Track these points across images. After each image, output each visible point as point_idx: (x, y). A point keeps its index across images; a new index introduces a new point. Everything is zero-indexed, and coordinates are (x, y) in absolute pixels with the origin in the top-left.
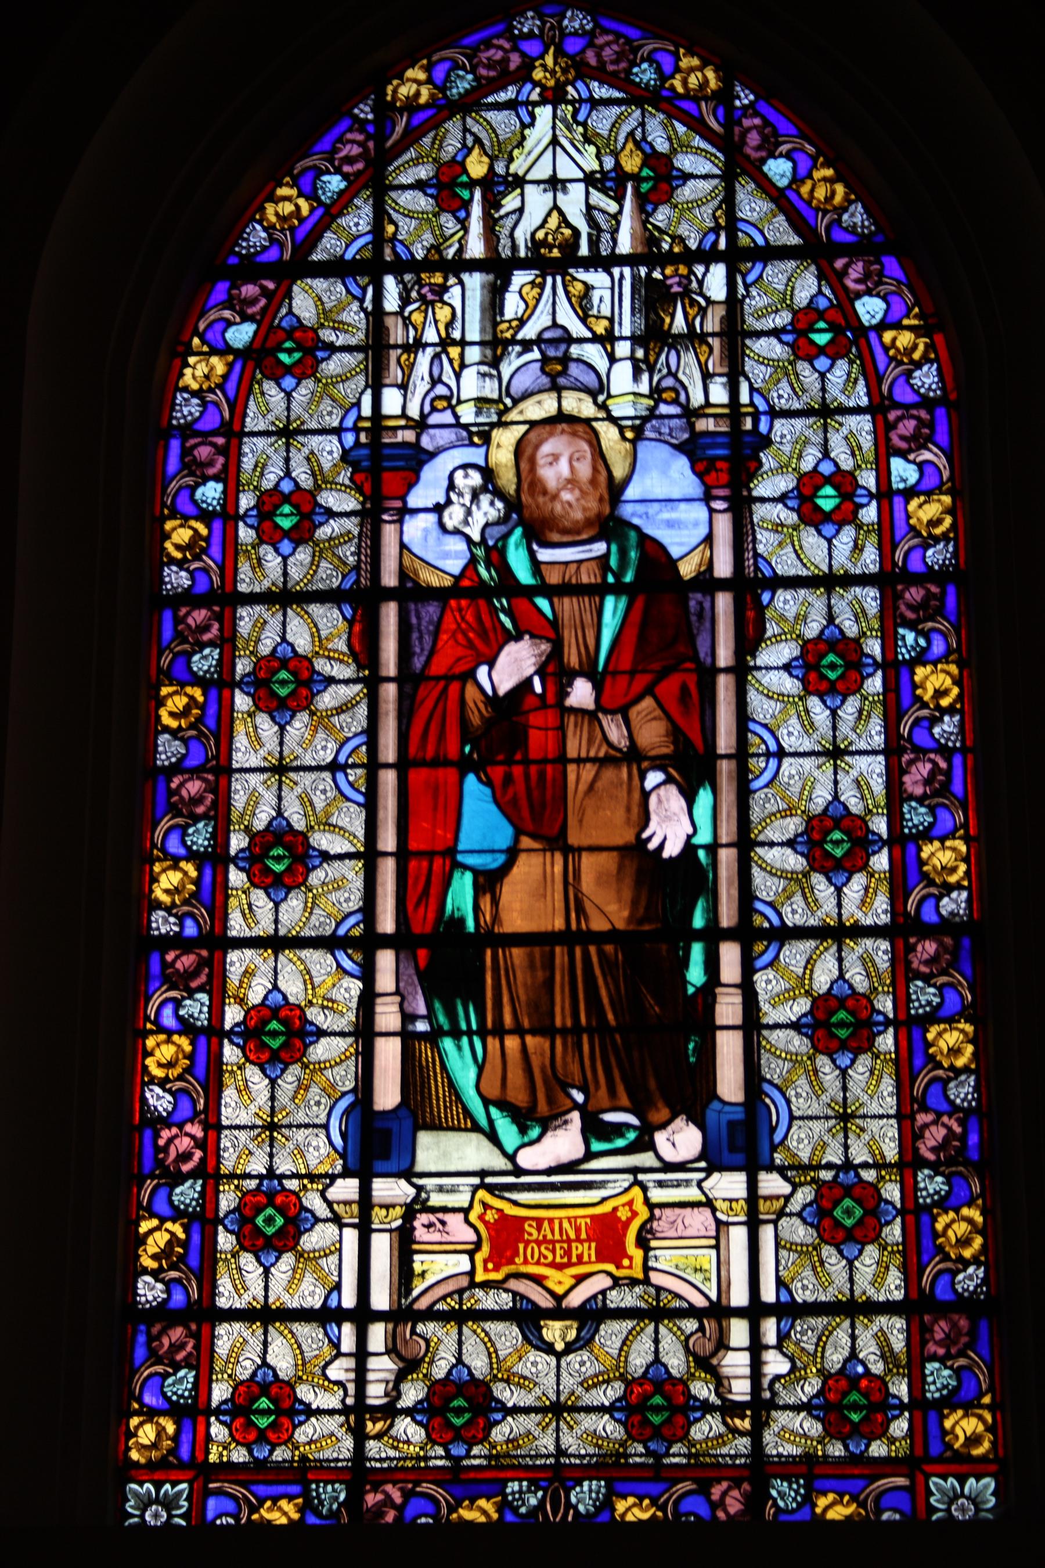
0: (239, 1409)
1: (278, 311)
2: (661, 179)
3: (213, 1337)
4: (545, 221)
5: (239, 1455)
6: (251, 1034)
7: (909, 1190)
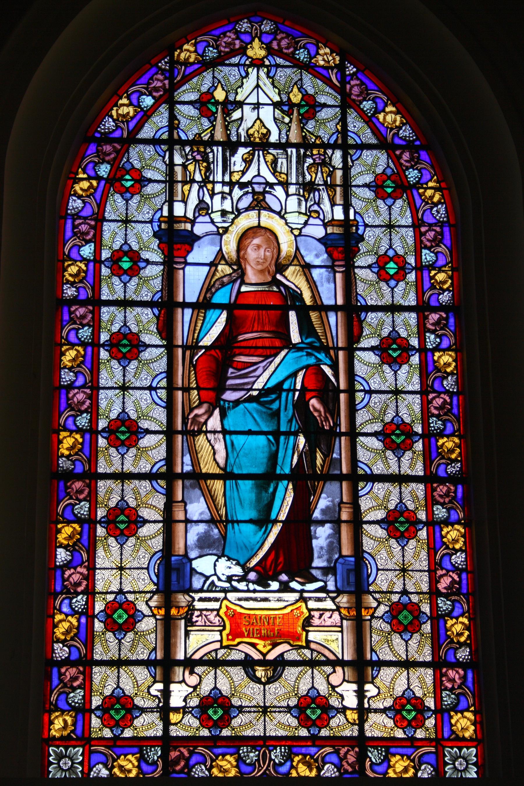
0: (106, 708)
1: (122, 160)
2: (311, 106)
3: (96, 487)
4: (253, 125)
5: (107, 733)
6: (110, 522)
7: (434, 606)
